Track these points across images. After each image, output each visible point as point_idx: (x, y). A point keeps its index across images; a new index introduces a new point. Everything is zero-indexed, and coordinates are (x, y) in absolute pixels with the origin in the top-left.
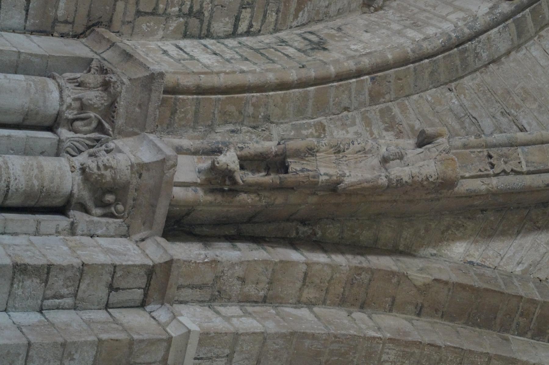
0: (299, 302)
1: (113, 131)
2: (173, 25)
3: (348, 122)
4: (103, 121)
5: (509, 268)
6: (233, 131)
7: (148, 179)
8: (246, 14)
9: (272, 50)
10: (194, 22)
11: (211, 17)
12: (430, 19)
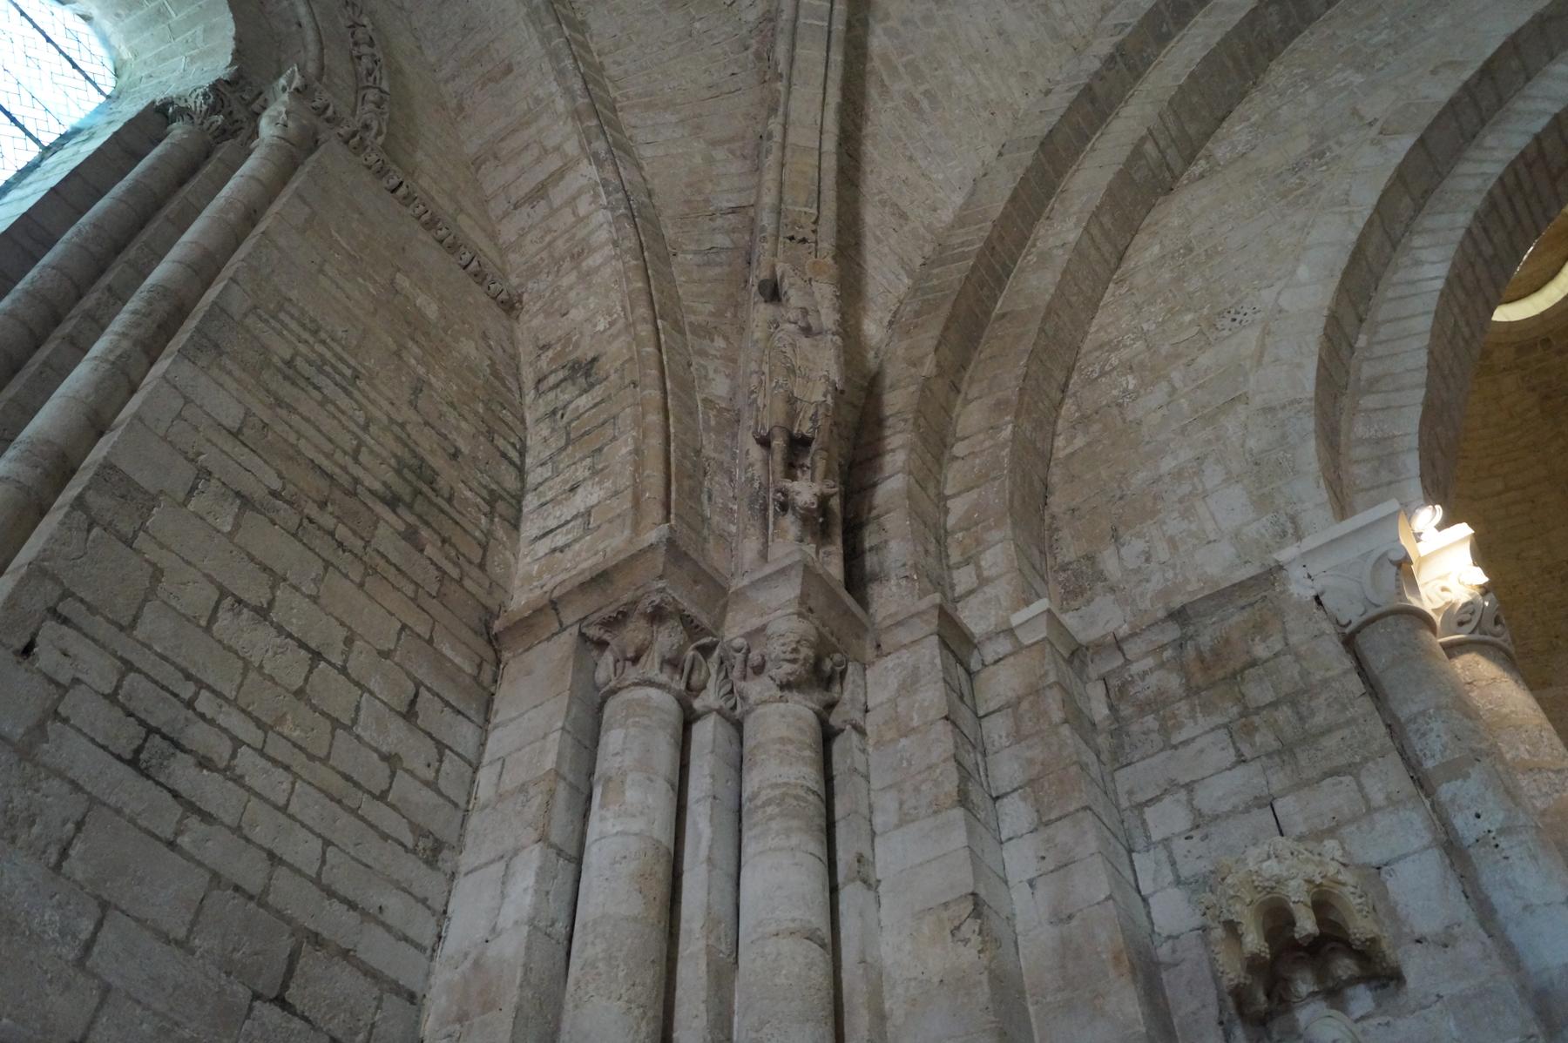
1: (714, 636)
2: (500, 533)
3: (703, 372)
4: (699, 643)
5: (903, 289)
6: (710, 498)
7: (817, 601)
8: (500, 442)
9: (573, 425)
10: (501, 506)
11: (497, 483)
12: (574, 235)
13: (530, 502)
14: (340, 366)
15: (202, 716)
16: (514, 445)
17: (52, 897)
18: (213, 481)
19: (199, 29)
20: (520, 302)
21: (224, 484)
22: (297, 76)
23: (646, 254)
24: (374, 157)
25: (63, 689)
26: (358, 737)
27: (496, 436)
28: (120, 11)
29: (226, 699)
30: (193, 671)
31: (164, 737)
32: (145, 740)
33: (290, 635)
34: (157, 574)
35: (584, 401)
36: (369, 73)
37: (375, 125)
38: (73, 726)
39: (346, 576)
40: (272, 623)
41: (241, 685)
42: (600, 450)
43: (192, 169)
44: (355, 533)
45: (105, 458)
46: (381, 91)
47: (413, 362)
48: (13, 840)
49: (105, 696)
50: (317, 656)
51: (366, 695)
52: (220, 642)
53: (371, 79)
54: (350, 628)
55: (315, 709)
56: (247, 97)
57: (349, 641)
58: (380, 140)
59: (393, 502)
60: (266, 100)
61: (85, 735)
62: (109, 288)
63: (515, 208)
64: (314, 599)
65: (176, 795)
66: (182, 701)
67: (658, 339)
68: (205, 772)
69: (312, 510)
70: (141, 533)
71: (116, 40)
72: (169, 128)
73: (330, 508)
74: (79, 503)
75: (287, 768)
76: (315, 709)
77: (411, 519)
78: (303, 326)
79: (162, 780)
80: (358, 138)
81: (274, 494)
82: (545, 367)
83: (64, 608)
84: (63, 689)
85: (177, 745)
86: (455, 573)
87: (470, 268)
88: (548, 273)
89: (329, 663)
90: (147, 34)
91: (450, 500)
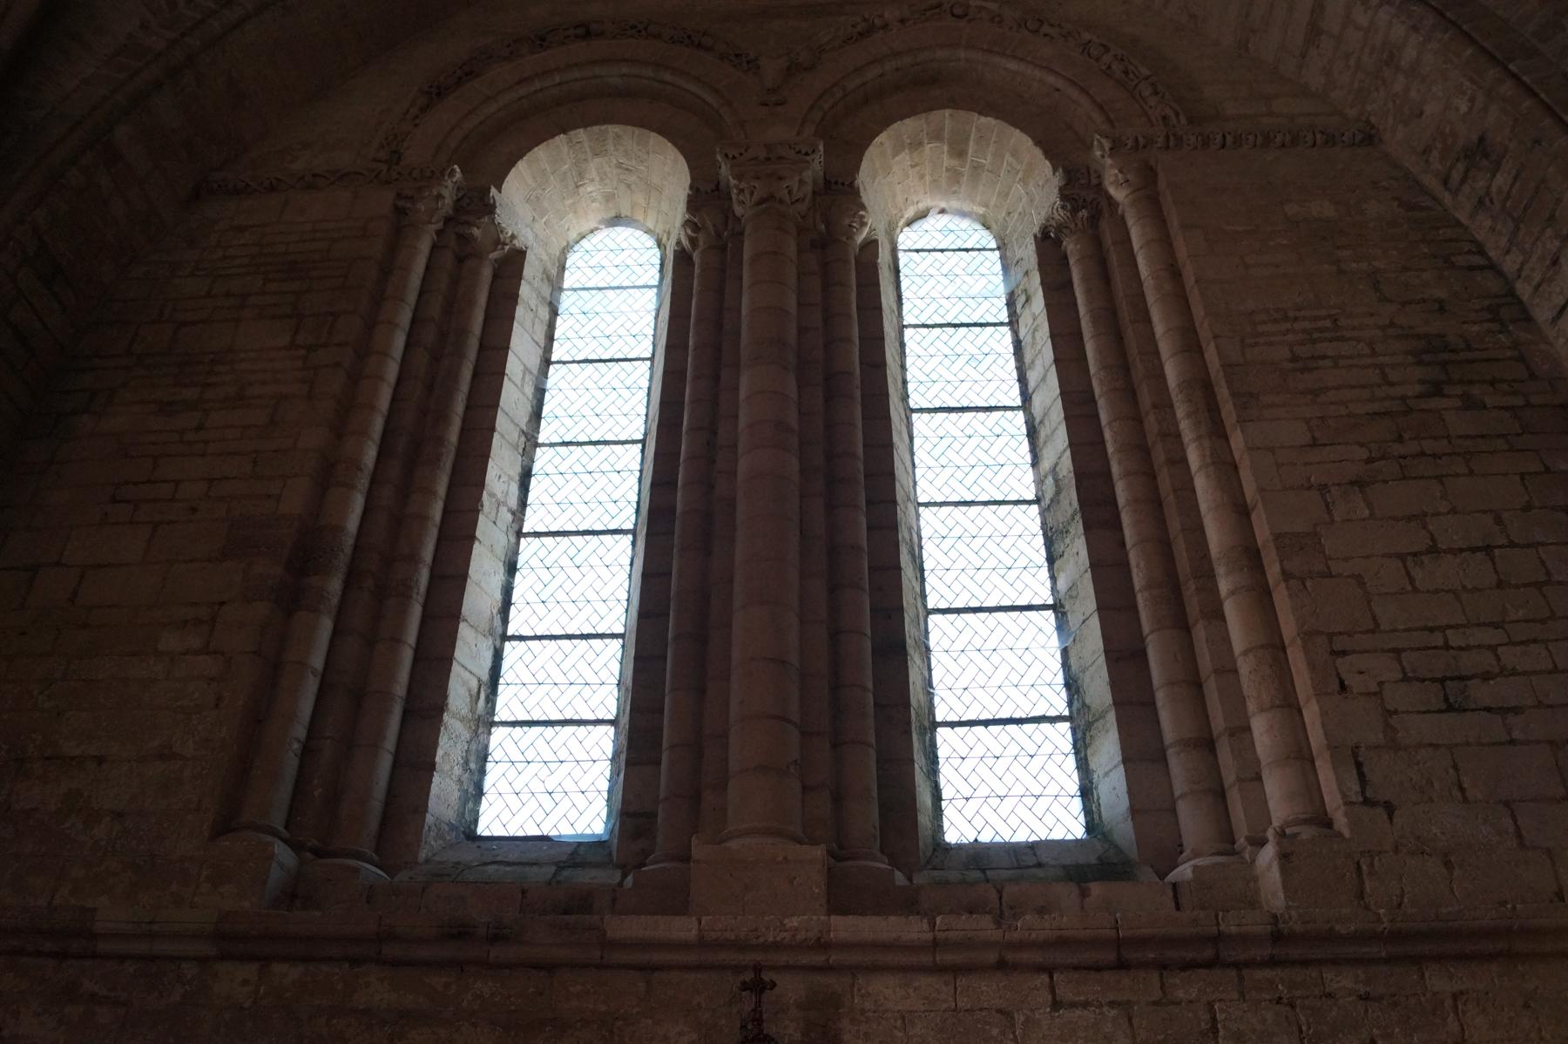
0: (1354, 144)
8: (1460, 260)
13: (1524, 290)
14: (1320, 324)
15: (1461, 648)
16: (1470, 252)
17: (1477, 818)
18: (1332, 489)
19: (1008, 157)
20: (1373, 127)
21: (1338, 484)
22: (1104, 141)
23: (1448, 14)
24: (1193, 139)
25: (1378, 694)
26: (1560, 583)
27: (1453, 259)
28: (954, 189)
29: (1463, 626)
30: (1430, 624)
31: (1452, 679)
32: (1444, 689)
33: (1462, 550)
34: (1359, 579)
35: (1501, 180)
36: (1126, 73)
37: (1169, 112)
38: (1403, 712)
39: (1457, 475)
40: (1444, 552)
41: (1464, 610)
42: (1552, 217)
43: (1103, 263)
44: (1435, 438)
45: (1271, 533)
46: (1147, 78)
47: (1354, 265)
48: (1431, 800)
49: (1402, 680)
50: (1488, 549)
51: (1540, 549)
52: (1428, 591)
53: (1131, 76)
54: (1491, 511)
55: (1517, 587)
56: (1083, 182)
57: (1499, 520)
58: (1183, 120)
59: (1436, 390)
60: (1095, 171)
61: (1411, 712)
62: (1155, 406)
63: (1304, 58)
64: (1453, 511)
65: (1488, 709)
66: (1441, 648)
67: (1524, 84)
68: (1492, 682)
69: (1397, 449)
70: (1329, 562)
71: (966, 207)
72: (1063, 248)
73: (1406, 436)
74: (1286, 575)
75: (1535, 641)
76: (1517, 587)
77: (1458, 390)
78: (1276, 321)
79: (1473, 706)
80: (1172, 138)
81: (1370, 461)
82: (1440, 167)
83: (1337, 647)
84: (1378, 694)
85: (1461, 678)
86: (1519, 401)
87: (1318, 142)
88: (1377, 89)
89: (1500, 547)
90: (981, 187)
91: (1469, 348)
